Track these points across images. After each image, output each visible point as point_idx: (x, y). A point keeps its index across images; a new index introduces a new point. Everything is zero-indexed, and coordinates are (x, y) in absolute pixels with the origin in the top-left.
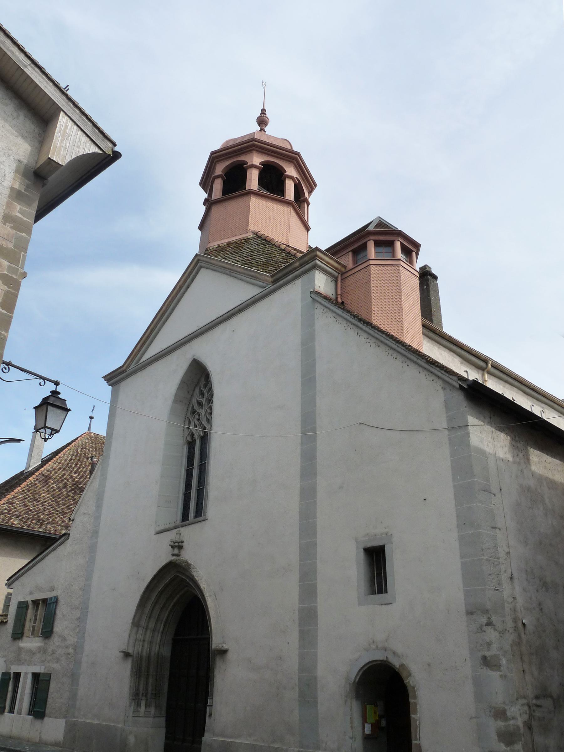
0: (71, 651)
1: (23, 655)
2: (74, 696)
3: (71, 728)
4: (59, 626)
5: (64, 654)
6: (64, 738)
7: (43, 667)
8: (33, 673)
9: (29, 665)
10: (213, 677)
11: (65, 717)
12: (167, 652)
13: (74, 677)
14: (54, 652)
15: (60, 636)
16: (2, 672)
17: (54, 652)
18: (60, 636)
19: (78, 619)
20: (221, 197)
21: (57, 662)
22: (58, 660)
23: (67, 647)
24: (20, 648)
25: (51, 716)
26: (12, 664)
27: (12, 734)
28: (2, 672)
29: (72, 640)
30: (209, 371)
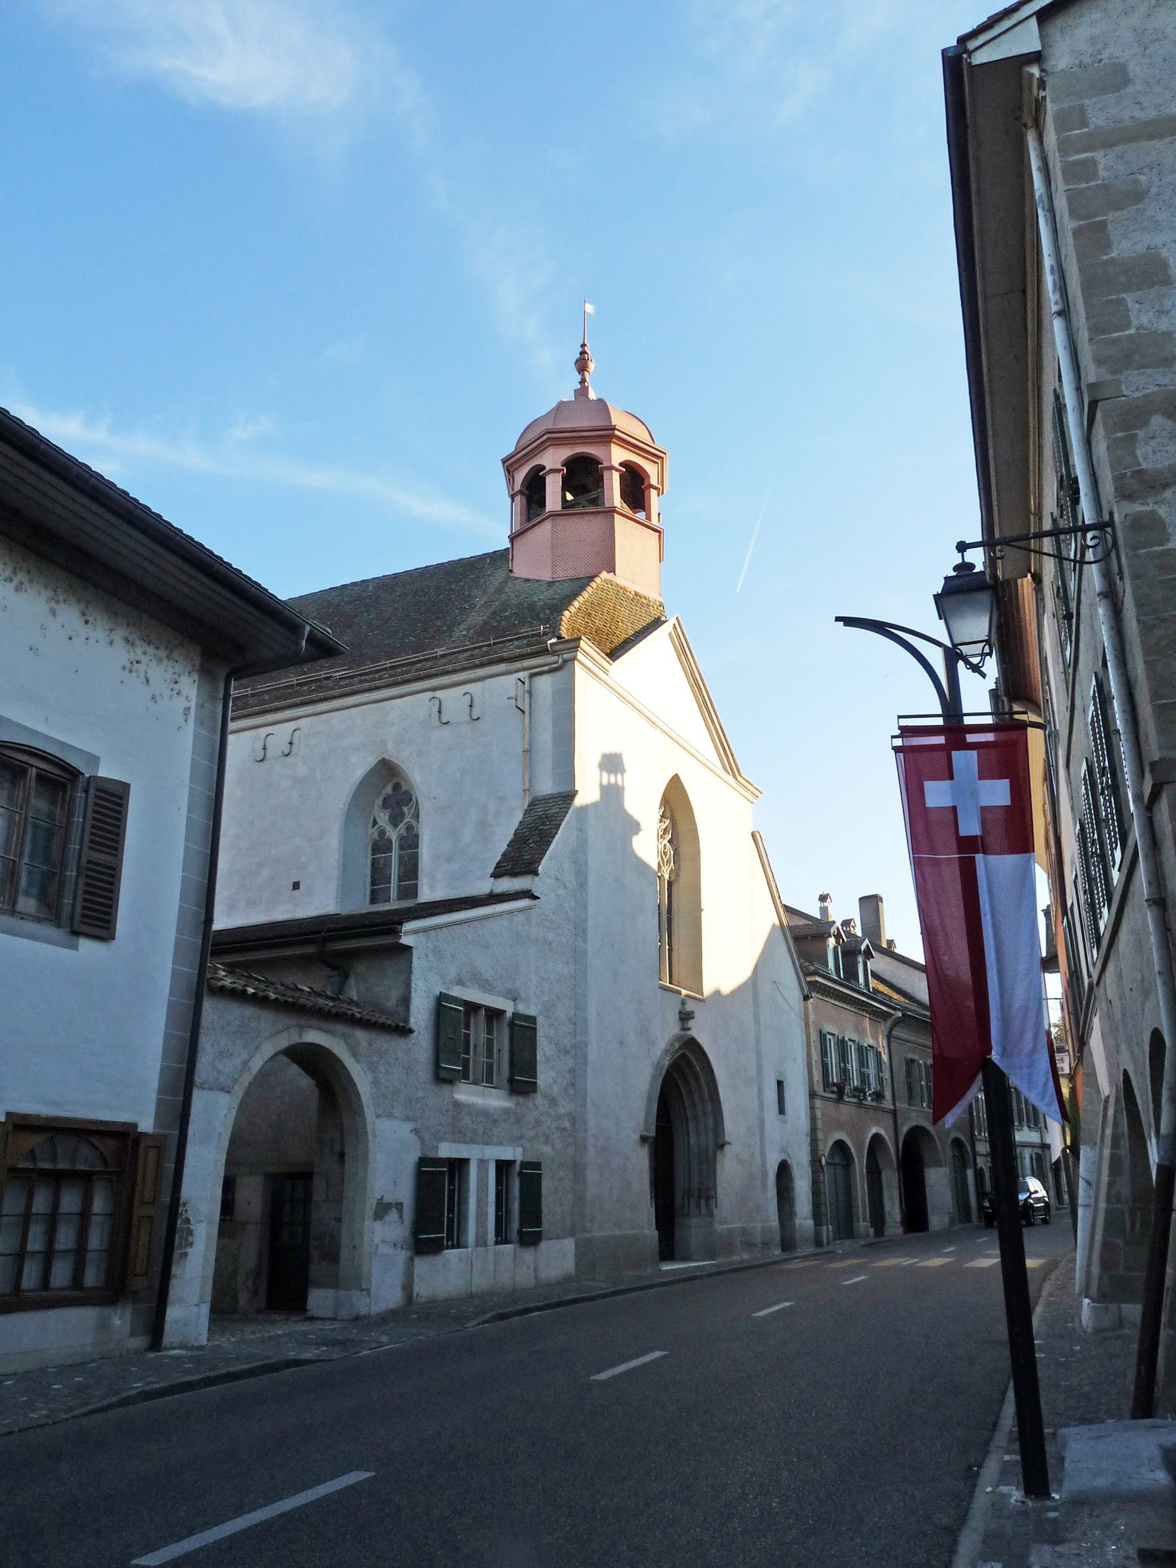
0: (567, 1125)
1: (467, 1120)
2: (580, 1199)
3: (584, 1251)
4: (545, 1077)
5: (557, 1128)
6: (577, 1265)
7: (520, 1150)
8: (497, 1161)
9: (486, 1144)
10: (651, 1160)
11: (572, 1233)
12: (926, 1170)
13: (578, 1171)
14: (538, 1123)
15: (545, 1096)
16: (126, 787)
17: (538, 1123)
18: (545, 1096)
19: (572, 1071)
20: (485, 886)
21: (546, 1142)
22: (547, 1140)
23: (559, 1117)
24: (457, 1104)
25: (944, 1520)
26: (441, 1140)
27: (474, 1289)
28: (126, 787)
29: (564, 1107)
30: (1076, 411)
